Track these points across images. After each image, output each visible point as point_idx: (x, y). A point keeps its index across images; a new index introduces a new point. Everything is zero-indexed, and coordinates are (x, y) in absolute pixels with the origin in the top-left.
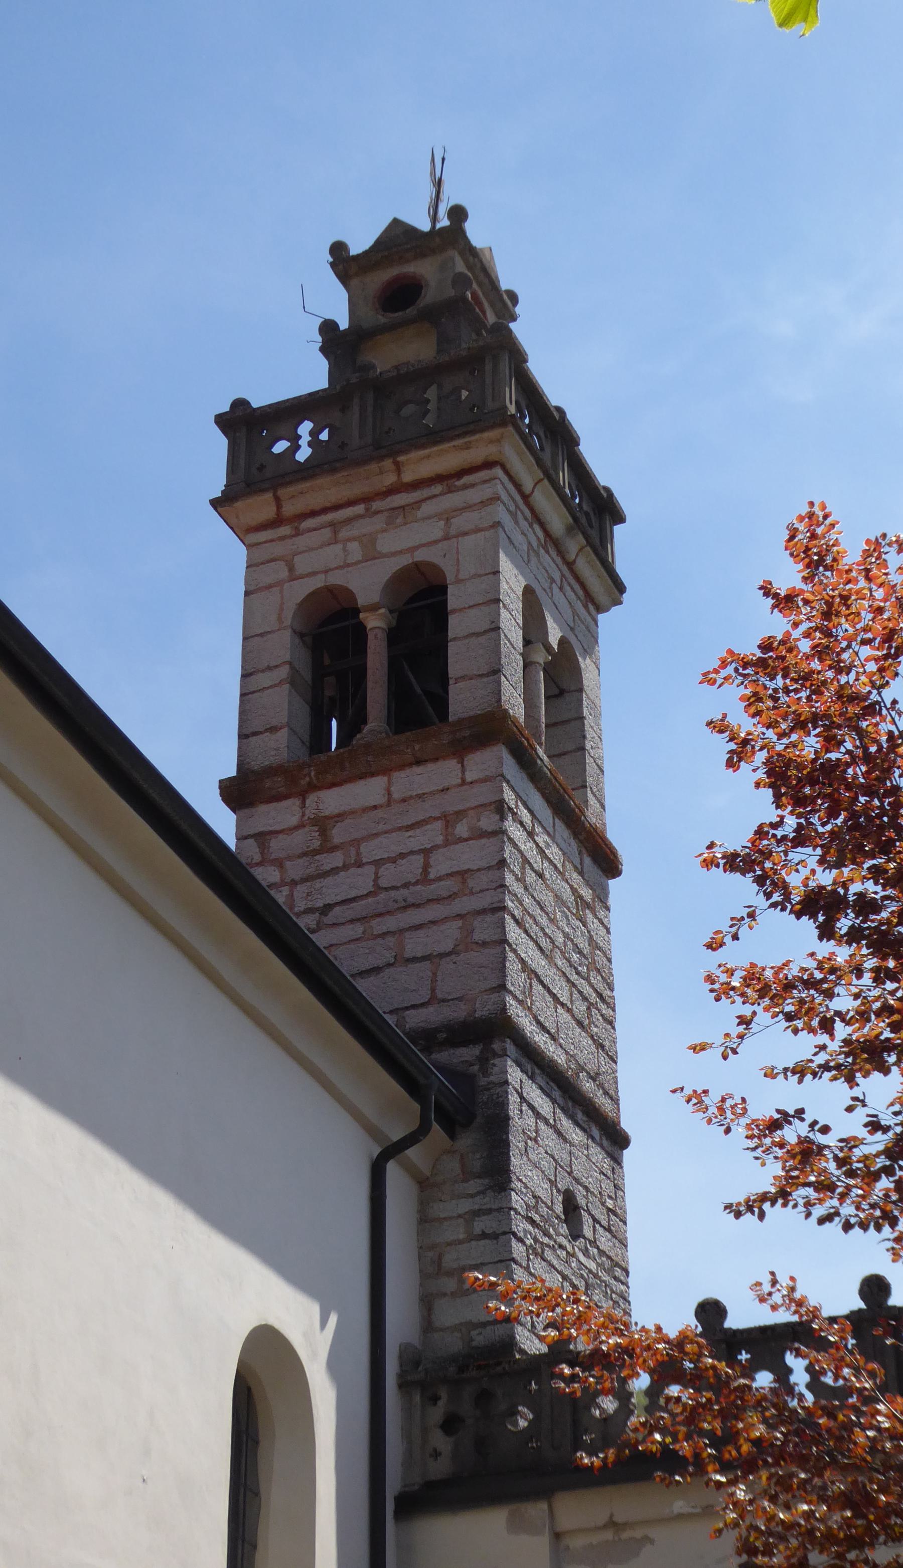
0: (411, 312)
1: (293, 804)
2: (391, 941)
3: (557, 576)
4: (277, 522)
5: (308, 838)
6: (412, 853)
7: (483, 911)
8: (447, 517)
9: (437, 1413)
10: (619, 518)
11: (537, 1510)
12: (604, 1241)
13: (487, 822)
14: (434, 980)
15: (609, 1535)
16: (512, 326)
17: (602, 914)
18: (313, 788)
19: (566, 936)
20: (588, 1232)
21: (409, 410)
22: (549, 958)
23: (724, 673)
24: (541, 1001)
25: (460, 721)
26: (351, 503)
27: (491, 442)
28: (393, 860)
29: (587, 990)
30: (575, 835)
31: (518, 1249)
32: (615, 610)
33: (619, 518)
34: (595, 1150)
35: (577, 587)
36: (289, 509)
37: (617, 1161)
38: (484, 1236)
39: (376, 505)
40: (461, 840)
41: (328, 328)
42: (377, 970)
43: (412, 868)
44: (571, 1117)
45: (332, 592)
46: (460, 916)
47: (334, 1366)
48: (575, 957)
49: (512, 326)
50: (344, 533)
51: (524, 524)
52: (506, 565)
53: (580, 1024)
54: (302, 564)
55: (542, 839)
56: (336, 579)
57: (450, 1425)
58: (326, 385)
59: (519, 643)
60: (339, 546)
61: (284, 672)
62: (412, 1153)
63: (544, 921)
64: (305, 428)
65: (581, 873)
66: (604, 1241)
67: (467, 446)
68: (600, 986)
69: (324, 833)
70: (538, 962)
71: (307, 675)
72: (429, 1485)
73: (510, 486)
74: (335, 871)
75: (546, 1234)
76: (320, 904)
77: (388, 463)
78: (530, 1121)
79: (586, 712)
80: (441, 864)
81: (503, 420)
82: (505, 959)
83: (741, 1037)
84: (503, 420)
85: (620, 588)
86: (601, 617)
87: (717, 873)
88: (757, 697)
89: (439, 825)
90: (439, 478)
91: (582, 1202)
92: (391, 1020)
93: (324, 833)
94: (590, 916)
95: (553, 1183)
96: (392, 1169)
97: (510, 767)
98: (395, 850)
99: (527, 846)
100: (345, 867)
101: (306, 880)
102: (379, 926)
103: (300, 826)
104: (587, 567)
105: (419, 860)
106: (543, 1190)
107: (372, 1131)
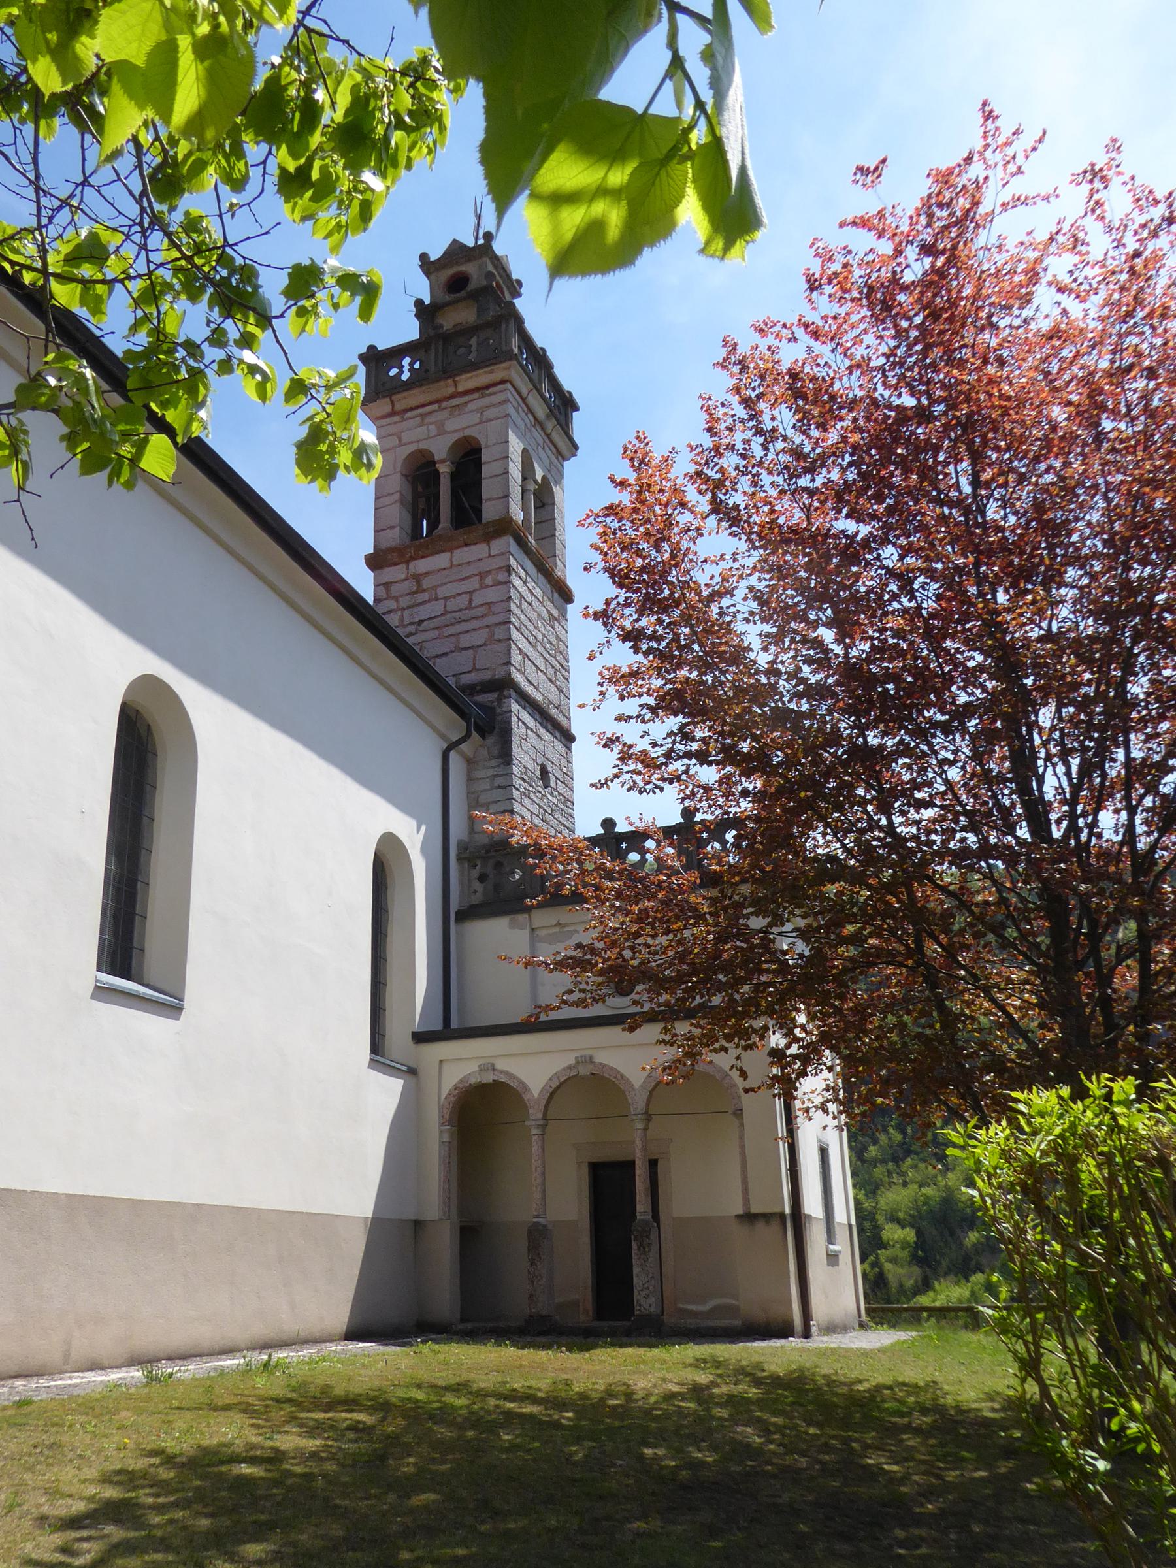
0: (463, 293)
2: (453, 639)
3: (541, 442)
4: (393, 413)
5: (410, 585)
7: (500, 624)
8: (481, 411)
9: (476, 873)
10: (576, 408)
11: (522, 918)
13: (502, 577)
14: (474, 659)
15: (557, 929)
16: (517, 301)
17: (563, 623)
18: (413, 558)
19: (544, 635)
20: (553, 784)
21: (462, 351)
22: (534, 647)
23: (589, 521)
24: (530, 669)
25: (488, 523)
26: (430, 403)
27: (505, 369)
28: (454, 597)
29: (555, 663)
30: (549, 582)
31: (516, 794)
32: (573, 459)
33: (576, 408)
35: (552, 448)
36: (398, 407)
37: (569, 749)
38: (499, 787)
39: (444, 404)
40: (488, 586)
41: (419, 303)
42: (446, 654)
43: (463, 601)
44: (545, 727)
45: (421, 452)
46: (487, 626)
47: (424, 850)
48: (548, 646)
49: (517, 301)
50: (428, 420)
51: (523, 414)
52: (513, 438)
53: (550, 680)
54: (406, 437)
55: (531, 585)
57: (482, 878)
58: (418, 337)
59: (520, 480)
60: (424, 428)
61: (397, 496)
62: (463, 746)
63: (531, 628)
64: (406, 361)
65: (552, 602)
67: (492, 372)
68: (562, 661)
69: (418, 582)
70: (528, 649)
71: (409, 498)
72: (472, 906)
73: (515, 393)
74: (424, 603)
75: (531, 786)
76: (417, 620)
77: (450, 381)
78: (523, 730)
79: (556, 515)
80: (478, 600)
81: (510, 357)
82: (510, 648)
83: (601, 701)
84: (510, 357)
85: (576, 447)
86: (566, 464)
87: (590, 620)
88: (605, 533)
89: (477, 578)
90: (477, 389)
91: (550, 769)
92: (452, 681)
93: (418, 582)
94: (556, 623)
95: (535, 761)
96: (452, 754)
97: (514, 547)
98: (454, 592)
100: (429, 601)
101: (409, 607)
102: (448, 631)
103: (406, 579)
104: (558, 437)
105: (466, 597)
106: (530, 764)
107: (443, 737)
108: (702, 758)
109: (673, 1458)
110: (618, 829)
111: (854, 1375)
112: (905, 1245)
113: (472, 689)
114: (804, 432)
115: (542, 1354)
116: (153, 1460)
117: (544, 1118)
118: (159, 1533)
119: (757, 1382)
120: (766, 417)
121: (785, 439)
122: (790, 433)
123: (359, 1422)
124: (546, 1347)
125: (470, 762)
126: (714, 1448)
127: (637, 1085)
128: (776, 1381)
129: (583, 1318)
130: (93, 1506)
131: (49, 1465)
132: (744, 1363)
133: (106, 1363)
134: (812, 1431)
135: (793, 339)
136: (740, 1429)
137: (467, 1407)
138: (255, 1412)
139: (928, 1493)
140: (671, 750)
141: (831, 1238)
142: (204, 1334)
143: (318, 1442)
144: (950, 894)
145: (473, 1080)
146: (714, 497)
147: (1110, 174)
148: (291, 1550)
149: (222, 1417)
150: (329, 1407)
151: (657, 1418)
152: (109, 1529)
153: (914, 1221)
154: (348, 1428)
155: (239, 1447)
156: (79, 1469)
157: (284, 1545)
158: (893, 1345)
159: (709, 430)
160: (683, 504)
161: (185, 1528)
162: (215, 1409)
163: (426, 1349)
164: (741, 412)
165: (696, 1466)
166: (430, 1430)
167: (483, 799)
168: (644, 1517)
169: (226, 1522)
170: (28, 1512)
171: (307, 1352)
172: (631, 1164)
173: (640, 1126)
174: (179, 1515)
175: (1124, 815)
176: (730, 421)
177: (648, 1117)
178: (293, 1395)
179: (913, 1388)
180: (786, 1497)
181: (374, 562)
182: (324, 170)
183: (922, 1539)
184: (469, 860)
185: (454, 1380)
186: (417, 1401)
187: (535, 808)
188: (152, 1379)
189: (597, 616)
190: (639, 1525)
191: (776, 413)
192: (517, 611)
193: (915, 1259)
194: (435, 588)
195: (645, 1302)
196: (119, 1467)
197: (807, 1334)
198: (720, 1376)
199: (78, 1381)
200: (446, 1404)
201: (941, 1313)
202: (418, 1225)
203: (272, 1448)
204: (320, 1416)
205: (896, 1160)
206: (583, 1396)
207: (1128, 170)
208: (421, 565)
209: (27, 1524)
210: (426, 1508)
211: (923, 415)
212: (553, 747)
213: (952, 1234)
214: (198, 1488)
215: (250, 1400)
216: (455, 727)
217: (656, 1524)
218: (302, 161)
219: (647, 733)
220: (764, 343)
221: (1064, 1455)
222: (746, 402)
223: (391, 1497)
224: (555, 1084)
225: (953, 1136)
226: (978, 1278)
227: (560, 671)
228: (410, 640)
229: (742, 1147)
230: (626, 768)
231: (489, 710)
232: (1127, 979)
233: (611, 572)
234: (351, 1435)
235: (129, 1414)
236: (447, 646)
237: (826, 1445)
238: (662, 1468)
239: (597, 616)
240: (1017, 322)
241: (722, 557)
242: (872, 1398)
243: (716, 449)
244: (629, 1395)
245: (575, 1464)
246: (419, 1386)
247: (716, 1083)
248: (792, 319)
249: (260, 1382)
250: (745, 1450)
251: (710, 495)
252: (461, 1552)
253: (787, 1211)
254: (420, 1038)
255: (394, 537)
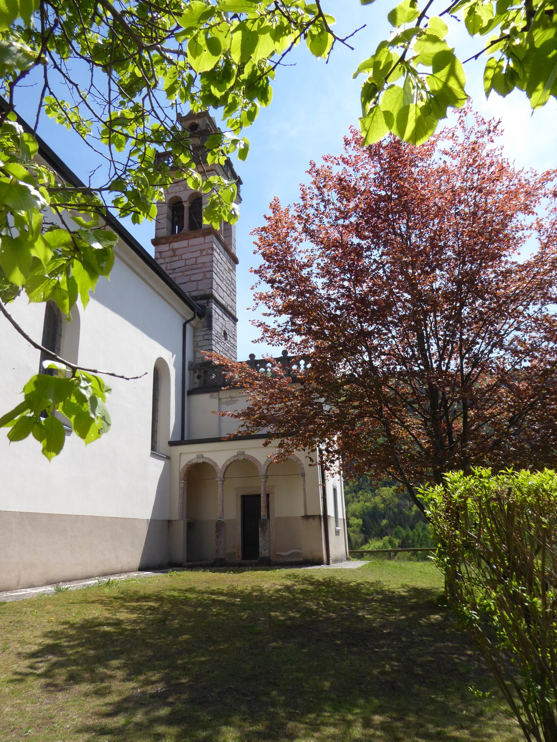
1: (167, 245)
5: (171, 253)
6: (333, 43)
9: (196, 375)
11: (216, 394)
12: (232, 341)
18: (172, 242)
31: (214, 342)
34: (231, 322)
37: (235, 324)
45: (177, 197)
47: (175, 365)
56: (177, 195)
57: (199, 377)
61: (166, 215)
66: (232, 341)
69: (174, 252)
70: (220, 282)
71: (171, 216)
78: (217, 316)
80: (200, 260)
92: (188, 294)
93: (174, 252)
96: (188, 325)
97: (215, 239)
99: (218, 257)
102: (186, 273)
106: (219, 330)
107: (184, 318)
108: (298, 332)
109: (283, 616)
110: (256, 358)
111: (349, 579)
112: (358, 525)
113: (196, 298)
114: (340, 202)
115: (223, 575)
116: (65, 626)
117: (224, 477)
118: (73, 658)
119: (312, 584)
120: (326, 194)
121: (333, 204)
122: (335, 202)
123: (151, 606)
124: (224, 571)
125: (194, 329)
126: (298, 611)
127: (262, 464)
128: (318, 584)
129: (237, 559)
130: (41, 647)
131: (18, 630)
132: (306, 576)
133: (36, 584)
134: (336, 602)
135: (338, 164)
136: (308, 603)
137: (196, 598)
138: (105, 603)
139: (384, 626)
140: (286, 329)
141: (337, 526)
142: (79, 570)
143: (136, 615)
144: (392, 389)
145: (194, 462)
146: (305, 225)
147: (467, 111)
148: (131, 662)
149: (92, 606)
150: (138, 600)
151: (274, 600)
152: (50, 657)
153: (362, 516)
154: (147, 609)
155: (101, 619)
156: (32, 631)
157: (128, 660)
158: (363, 566)
159: (302, 198)
160: (293, 228)
161: (83, 655)
162: (89, 603)
163: (174, 574)
164: (316, 192)
165: (292, 619)
166: (182, 608)
167: (200, 344)
168: (275, 641)
169: (101, 651)
170: (12, 651)
171: (123, 577)
172: (259, 496)
173: (263, 480)
174: (80, 649)
175: (459, 360)
176: (312, 195)
177: (266, 476)
178: (122, 596)
179: (372, 584)
180: (330, 630)
181: (155, 242)
182: (234, 99)
183: (384, 644)
184: (193, 369)
185: (188, 587)
186: (174, 596)
187: (221, 349)
188: (59, 591)
189: (256, 272)
190: (274, 644)
191: (330, 193)
192: (216, 266)
193: (362, 531)
194: (181, 255)
195: (264, 552)
196: (50, 630)
197: (328, 564)
198: (296, 582)
199: (24, 593)
200: (187, 597)
201: (371, 553)
202: (169, 522)
203: (116, 619)
204: (135, 604)
205: (356, 492)
206: (242, 592)
207: (474, 110)
208: (176, 245)
209: (13, 657)
210: (186, 642)
211: (388, 199)
212: (229, 323)
213: (376, 521)
214: (87, 638)
215: (103, 598)
216: (189, 314)
217: (280, 643)
218: (223, 93)
219: (276, 321)
220: (326, 164)
221: (464, 613)
222: (319, 188)
223: (170, 638)
224: (228, 463)
225: (420, 490)
226: (386, 538)
227: (232, 292)
228: (170, 276)
229: (304, 489)
230: (266, 335)
231: (202, 307)
232: (458, 424)
233: (264, 255)
234: (149, 612)
235: (50, 607)
236: (186, 279)
237: (342, 608)
238: (279, 620)
239: (256, 272)
240: (425, 165)
241: (307, 251)
242: (357, 589)
243: (305, 206)
244: (261, 590)
245: (244, 620)
246: (174, 590)
247: (297, 463)
248: (338, 156)
249: (107, 590)
250: (310, 612)
251: (303, 225)
252: (203, 659)
253: (322, 514)
254: (172, 444)
255: (164, 233)
